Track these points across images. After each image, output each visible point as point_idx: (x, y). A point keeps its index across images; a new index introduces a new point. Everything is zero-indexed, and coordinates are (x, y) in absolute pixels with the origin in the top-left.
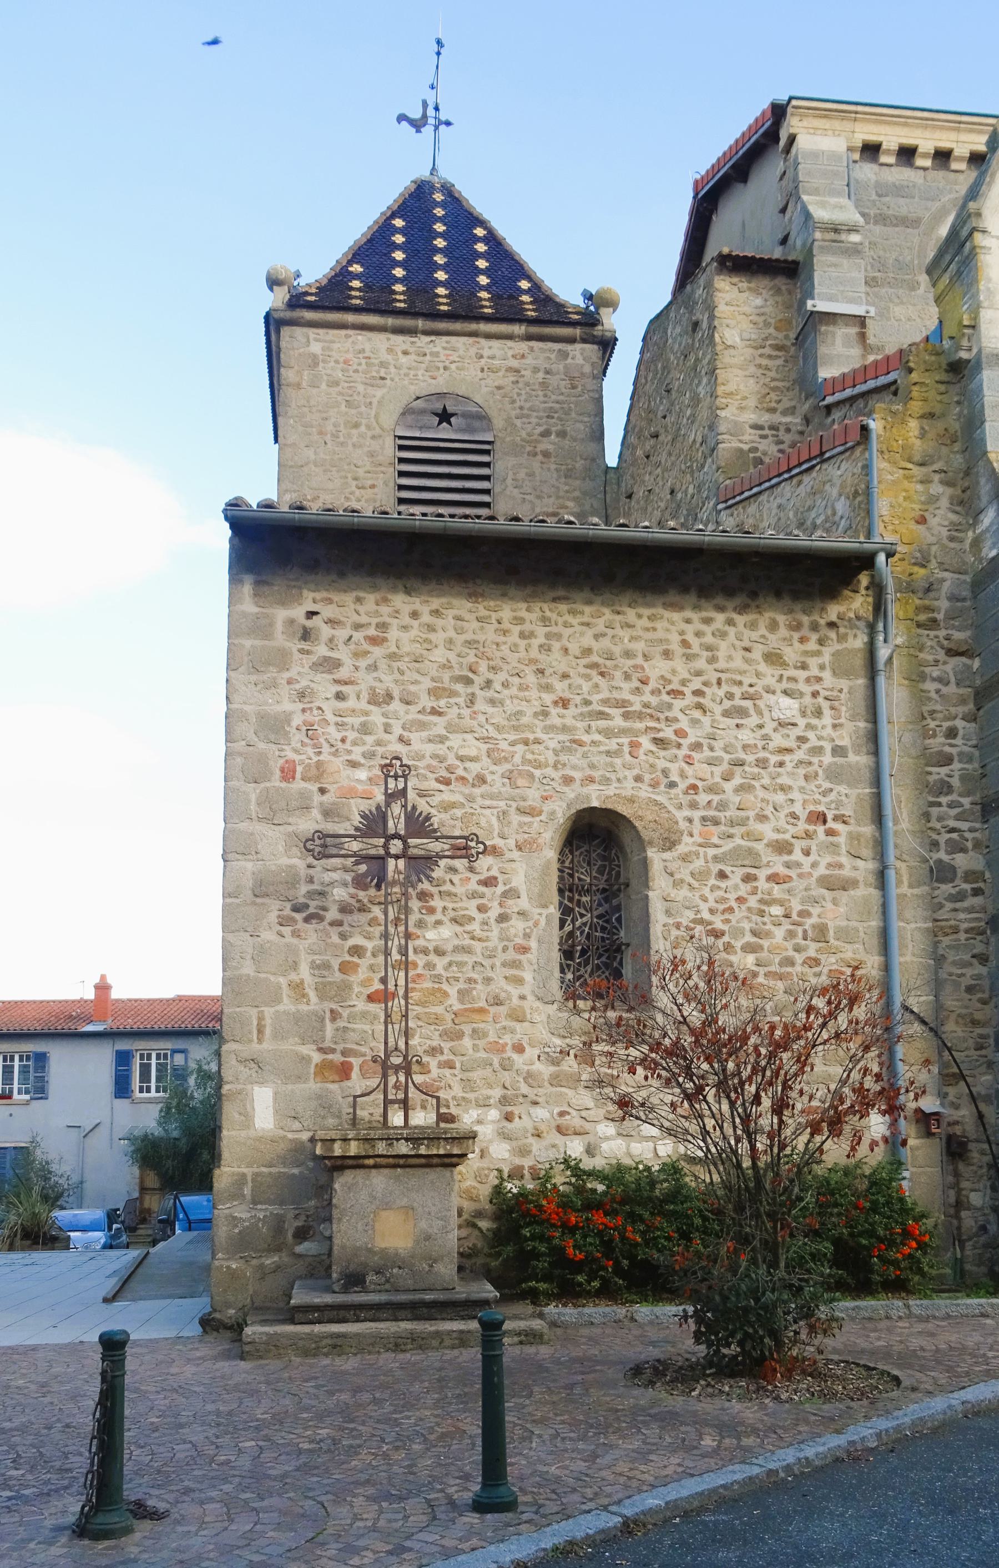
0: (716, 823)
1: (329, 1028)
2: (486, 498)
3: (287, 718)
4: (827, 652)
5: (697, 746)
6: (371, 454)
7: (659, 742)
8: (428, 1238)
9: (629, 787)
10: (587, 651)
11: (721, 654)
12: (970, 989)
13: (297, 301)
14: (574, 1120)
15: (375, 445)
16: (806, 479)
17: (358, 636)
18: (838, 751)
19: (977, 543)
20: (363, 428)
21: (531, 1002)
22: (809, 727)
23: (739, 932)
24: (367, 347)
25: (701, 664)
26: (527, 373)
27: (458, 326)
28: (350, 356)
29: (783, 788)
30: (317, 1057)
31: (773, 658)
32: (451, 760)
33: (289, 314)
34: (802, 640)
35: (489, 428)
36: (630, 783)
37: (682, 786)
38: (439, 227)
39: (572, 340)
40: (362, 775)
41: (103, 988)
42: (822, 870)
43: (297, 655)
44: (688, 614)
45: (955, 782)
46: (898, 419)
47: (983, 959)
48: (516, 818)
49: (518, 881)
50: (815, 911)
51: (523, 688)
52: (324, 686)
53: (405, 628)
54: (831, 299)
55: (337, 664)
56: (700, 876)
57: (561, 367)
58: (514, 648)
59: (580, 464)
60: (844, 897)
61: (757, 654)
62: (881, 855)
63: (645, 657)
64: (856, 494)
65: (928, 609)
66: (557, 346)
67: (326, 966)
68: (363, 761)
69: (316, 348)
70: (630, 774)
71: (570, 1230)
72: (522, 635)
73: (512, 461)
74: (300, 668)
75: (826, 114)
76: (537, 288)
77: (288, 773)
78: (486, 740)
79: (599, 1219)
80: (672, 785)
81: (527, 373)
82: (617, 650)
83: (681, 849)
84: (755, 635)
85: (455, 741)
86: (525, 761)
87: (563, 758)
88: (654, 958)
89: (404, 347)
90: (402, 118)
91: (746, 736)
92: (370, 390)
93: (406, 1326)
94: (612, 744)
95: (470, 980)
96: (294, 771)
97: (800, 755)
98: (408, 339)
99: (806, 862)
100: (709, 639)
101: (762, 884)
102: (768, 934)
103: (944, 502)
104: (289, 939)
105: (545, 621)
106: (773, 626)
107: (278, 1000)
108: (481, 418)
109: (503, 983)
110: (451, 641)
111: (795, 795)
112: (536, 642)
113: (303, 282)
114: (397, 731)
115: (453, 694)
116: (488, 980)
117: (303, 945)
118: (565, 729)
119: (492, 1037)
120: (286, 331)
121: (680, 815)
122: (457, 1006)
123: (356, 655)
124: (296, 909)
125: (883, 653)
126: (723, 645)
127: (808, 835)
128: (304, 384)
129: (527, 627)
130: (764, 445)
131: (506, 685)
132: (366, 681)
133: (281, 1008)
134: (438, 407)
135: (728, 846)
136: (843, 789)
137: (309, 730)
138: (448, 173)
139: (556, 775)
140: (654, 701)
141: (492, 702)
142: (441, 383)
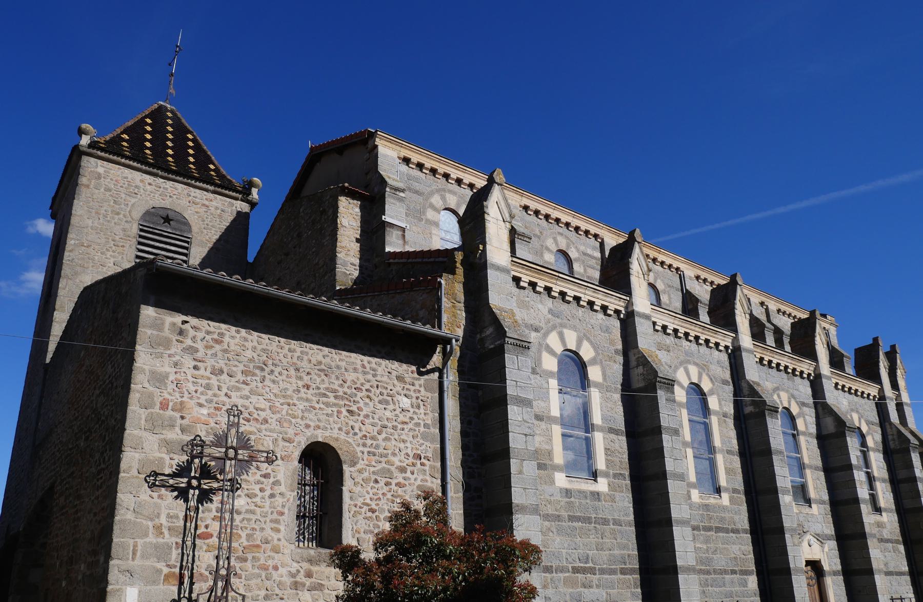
3: (167, 376)
5: (367, 416)
10: (320, 363)
15: (127, 226)
17: (208, 337)
18: (426, 426)
20: (121, 216)
21: (283, 542)
23: (382, 511)
24: (130, 176)
26: (212, 209)
28: (120, 178)
30: (166, 570)
31: (400, 378)
32: (251, 409)
35: (190, 231)
36: (336, 431)
37: (360, 435)
39: (236, 199)
40: (205, 411)
42: (419, 482)
43: (175, 342)
48: (281, 443)
49: (281, 477)
53: (233, 337)
55: (197, 351)
69: (101, 170)
70: (337, 426)
72: (290, 350)
74: (176, 348)
77: (164, 406)
78: (269, 400)
80: (355, 434)
81: (212, 209)
82: (333, 364)
83: (359, 466)
85: (254, 399)
86: (288, 414)
87: (306, 414)
91: (388, 414)
92: (128, 198)
94: (329, 411)
95: (253, 529)
98: (152, 178)
99: (412, 477)
101: (393, 486)
104: (156, 500)
107: (146, 535)
114: (225, 390)
115: (254, 375)
116: (262, 529)
117: (163, 504)
118: (307, 400)
119: (262, 561)
122: (245, 543)
123: (207, 347)
127: (414, 465)
128: (91, 186)
133: (148, 540)
135: (379, 467)
140: (349, 391)
141: (274, 382)
142: (167, 203)
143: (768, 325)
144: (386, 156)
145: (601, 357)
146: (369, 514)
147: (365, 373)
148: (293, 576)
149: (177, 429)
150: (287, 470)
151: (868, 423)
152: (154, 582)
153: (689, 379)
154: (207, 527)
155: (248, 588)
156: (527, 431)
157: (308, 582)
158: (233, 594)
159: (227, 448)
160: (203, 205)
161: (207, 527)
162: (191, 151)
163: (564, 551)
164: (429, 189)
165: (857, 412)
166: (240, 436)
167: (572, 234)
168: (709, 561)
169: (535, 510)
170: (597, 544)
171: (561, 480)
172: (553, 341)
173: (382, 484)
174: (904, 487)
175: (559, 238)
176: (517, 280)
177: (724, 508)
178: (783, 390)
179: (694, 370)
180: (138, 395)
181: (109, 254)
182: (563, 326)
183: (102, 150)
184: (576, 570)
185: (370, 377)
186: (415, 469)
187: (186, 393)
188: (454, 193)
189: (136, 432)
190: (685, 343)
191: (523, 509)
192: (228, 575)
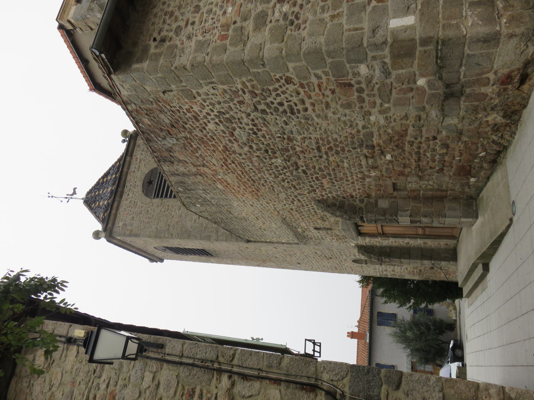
6: (158, 206)
20: (149, 209)
26: (142, 157)
28: (125, 213)
40: (230, 9)
41: (352, 335)
43: (172, 42)
57: (142, 147)
66: (136, 148)
68: (224, 10)
69: (121, 224)
81: (142, 157)
89: (126, 195)
92: (137, 207)
96: (223, 35)
104: (308, 24)
124: (292, 23)
128: (131, 228)
133: (344, 22)
142: (140, 184)
149: (245, 24)
160: (140, 162)
181: (173, 213)
187: (214, 25)
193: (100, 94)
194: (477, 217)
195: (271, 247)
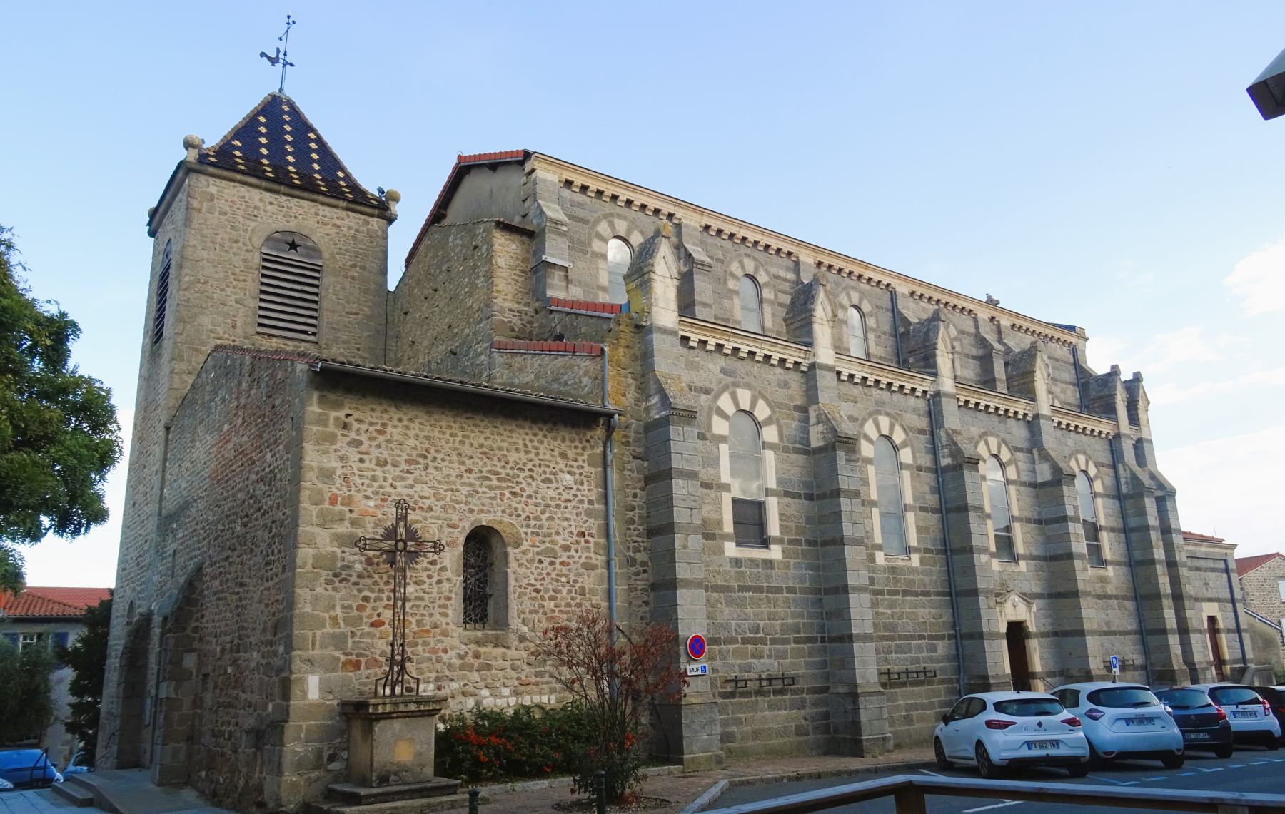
0: (538, 535)
1: (350, 641)
2: (315, 298)
3: (333, 471)
4: (586, 453)
5: (529, 497)
6: (245, 261)
7: (513, 494)
8: (421, 754)
9: (499, 516)
10: (481, 446)
11: (541, 451)
12: (642, 618)
13: (203, 158)
14: (470, 689)
15: (248, 256)
16: (560, 359)
17: (372, 429)
18: (590, 502)
19: (647, 409)
20: (240, 244)
21: (452, 626)
22: (578, 490)
23: (547, 590)
24: (247, 195)
25: (532, 456)
26: (345, 229)
27: (306, 195)
29: (568, 519)
30: (343, 658)
31: (563, 455)
32: (416, 498)
33: (198, 167)
34: (576, 447)
35: (320, 257)
36: (500, 514)
37: (523, 516)
38: (288, 128)
39: (372, 216)
40: (371, 503)
42: (583, 560)
43: (340, 437)
44: (527, 430)
45: (636, 519)
46: (615, 347)
47: (647, 603)
48: (446, 530)
49: (447, 563)
50: (580, 580)
51: (450, 462)
52: (354, 455)
53: (395, 427)
54: (553, 256)
55: (361, 443)
56: (531, 561)
58: (447, 441)
59: (372, 287)
60: (592, 573)
61: (556, 453)
62: (608, 553)
63: (508, 451)
64: (596, 378)
65: (626, 436)
66: (363, 217)
67: (350, 607)
69: (213, 190)
70: (500, 509)
71: (481, 746)
72: (451, 435)
73: (333, 279)
74: (341, 444)
75: (550, 163)
76: (348, 177)
77: (333, 501)
78: (433, 488)
79: (494, 740)
80: (519, 515)
81: (345, 229)
82: (495, 446)
83: (523, 548)
84: (556, 444)
85: (418, 487)
86: (452, 500)
87: (470, 499)
88: (299, 561)
90: (263, 54)
91: (551, 493)
92: (247, 222)
93: (424, 801)
94: (492, 494)
95: (423, 615)
97: (574, 503)
98: (274, 196)
99: (577, 555)
100: (536, 444)
101: (558, 566)
102: (560, 591)
103: (633, 388)
104: (331, 592)
105: (462, 429)
106: (563, 440)
107: (323, 626)
108: (315, 251)
109: (438, 616)
110: (417, 436)
111: (572, 523)
112: (458, 439)
113: (205, 146)
114: (390, 481)
115: (418, 463)
116: (431, 615)
117: (338, 595)
118: (470, 485)
119: (432, 645)
120: (193, 176)
121: (522, 530)
122: (416, 629)
123: (371, 439)
124: (335, 575)
125: (609, 457)
126: (542, 447)
127: (577, 543)
129: (454, 431)
130: (515, 320)
131: (443, 460)
132: (375, 453)
134: (290, 239)
135: (543, 547)
136: (592, 520)
137: (345, 478)
138: (290, 93)
139: (466, 508)
140: (511, 472)
141: (437, 468)
142: (292, 225)
143: (996, 345)
144: (545, 181)
145: (778, 415)
146: (534, 594)
147: (527, 452)
148: (461, 657)
149: (347, 523)
150: (452, 558)
151: (1097, 465)
152: (334, 670)
153: (879, 431)
154: (379, 615)
155: (420, 671)
156: (693, 504)
157: (476, 664)
158: (406, 677)
159: (397, 542)
160: (334, 225)
161: (379, 615)
162: (315, 156)
163: (733, 623)
164: (595, 216)
165: (1084, 453)
166: (408, 530)
167: (762, 257)
168: (892, 627)
169: (699, 585)
170: (769, 614)
171: (731, 549)
172: (725, 402)
173: (546, 563)
174: (1134, 537)
175: (746, 261)
176: (685, 340)
177: (913, 571)
178: (992, 435)
179: (884, 422)
180: (308, 492)
181: (229, 290)
182: (736, 385)
183: (212, 164)
184: (746, 641)
185: (532, 456)
186: (579, 547)
188: (624, 218)
189: (309, 529)
190: (876, 392)
191: (688, 584)
192: (403, 661)
193: (449, 179)
194: (159, 785)
195: (157, 466)
